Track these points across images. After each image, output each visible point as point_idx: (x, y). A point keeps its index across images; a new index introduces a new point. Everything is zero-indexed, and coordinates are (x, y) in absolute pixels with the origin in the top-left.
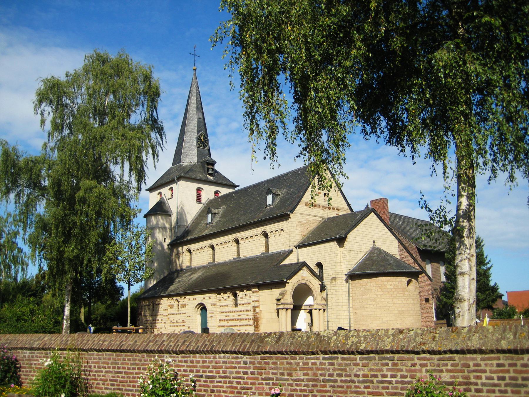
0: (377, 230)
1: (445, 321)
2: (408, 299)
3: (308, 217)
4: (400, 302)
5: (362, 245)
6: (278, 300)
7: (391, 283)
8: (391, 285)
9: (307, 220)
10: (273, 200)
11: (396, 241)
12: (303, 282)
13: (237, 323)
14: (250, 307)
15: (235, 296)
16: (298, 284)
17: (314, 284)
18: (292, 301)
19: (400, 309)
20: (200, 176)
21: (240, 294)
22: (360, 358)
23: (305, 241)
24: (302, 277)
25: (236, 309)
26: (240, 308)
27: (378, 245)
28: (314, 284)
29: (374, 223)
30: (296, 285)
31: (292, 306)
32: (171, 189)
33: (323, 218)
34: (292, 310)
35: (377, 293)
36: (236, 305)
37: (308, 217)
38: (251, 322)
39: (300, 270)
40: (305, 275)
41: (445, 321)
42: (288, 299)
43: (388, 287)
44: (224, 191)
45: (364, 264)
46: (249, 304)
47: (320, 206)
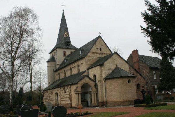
1: (141, 98)
2: (128, 88)
3: (93, 58)
4: (125, 89)
6: (75, 90)
7: (120, 81)
8: (121, 82)
9: (92, 59)
10: (82, 52)
11: (128, 65)
12: (86, 82)
13: (66, 99)
14: (69, 93)
15: (65, 89)
16: (83, 84)
17: (92, 83)
18: (81, 90)
19: (125, 92)
20: (64, 47)
21: (66, 88)
22: (47, 114)
23: (91, 67)
25: (65, 94)
26: (66, 93)
27: (119, 66)
28: (92, 83)
30: (83, 84)
31: (81, 93)
32: (55, 52)
33: (100, 58)
34: (81, 94)
35: (115, 86)
36: (65, 92)
37: (93, 58)
38: (69, 99)
39: (84, 78)
40: (87, 80)
41: (141, 98)
42: (79, 89)
43: (120, 83)
44: (73, 51)
45: (110, 74)
46: (68, 92)
47: (98, 53)
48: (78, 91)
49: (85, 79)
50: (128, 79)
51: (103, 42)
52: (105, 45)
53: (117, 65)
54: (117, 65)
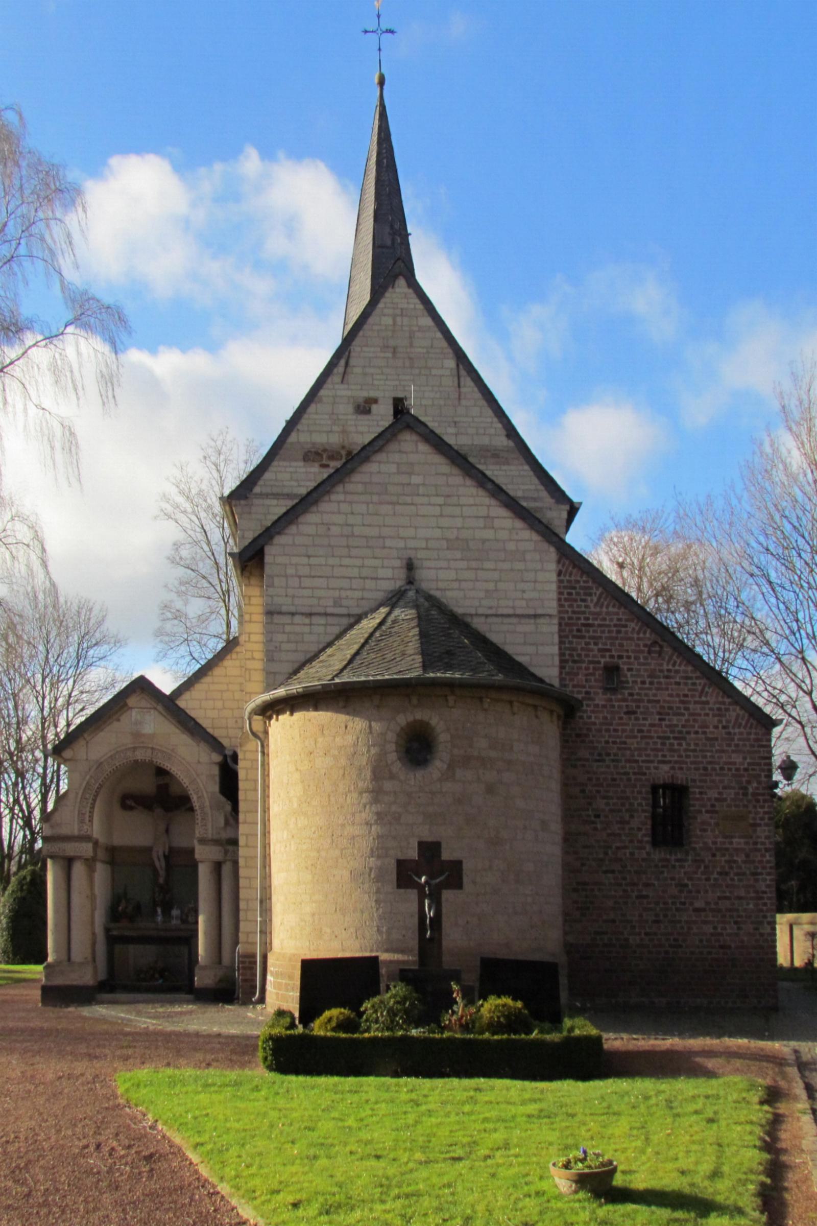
0: (437, 510)
5: (345, 583)
12: (140, 755)
24: (137, 735)
29: (416, 480)
48: (65, 831)
49: (135, 714)
50: (403, 720)
51: (428, 321)
52: (451, 363)
53: (410, 566)
54: (410, 566)
